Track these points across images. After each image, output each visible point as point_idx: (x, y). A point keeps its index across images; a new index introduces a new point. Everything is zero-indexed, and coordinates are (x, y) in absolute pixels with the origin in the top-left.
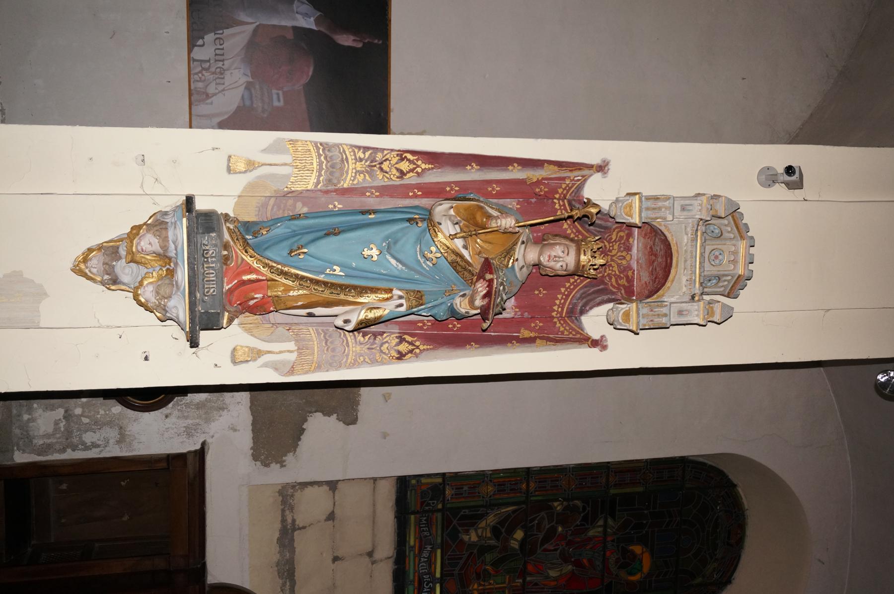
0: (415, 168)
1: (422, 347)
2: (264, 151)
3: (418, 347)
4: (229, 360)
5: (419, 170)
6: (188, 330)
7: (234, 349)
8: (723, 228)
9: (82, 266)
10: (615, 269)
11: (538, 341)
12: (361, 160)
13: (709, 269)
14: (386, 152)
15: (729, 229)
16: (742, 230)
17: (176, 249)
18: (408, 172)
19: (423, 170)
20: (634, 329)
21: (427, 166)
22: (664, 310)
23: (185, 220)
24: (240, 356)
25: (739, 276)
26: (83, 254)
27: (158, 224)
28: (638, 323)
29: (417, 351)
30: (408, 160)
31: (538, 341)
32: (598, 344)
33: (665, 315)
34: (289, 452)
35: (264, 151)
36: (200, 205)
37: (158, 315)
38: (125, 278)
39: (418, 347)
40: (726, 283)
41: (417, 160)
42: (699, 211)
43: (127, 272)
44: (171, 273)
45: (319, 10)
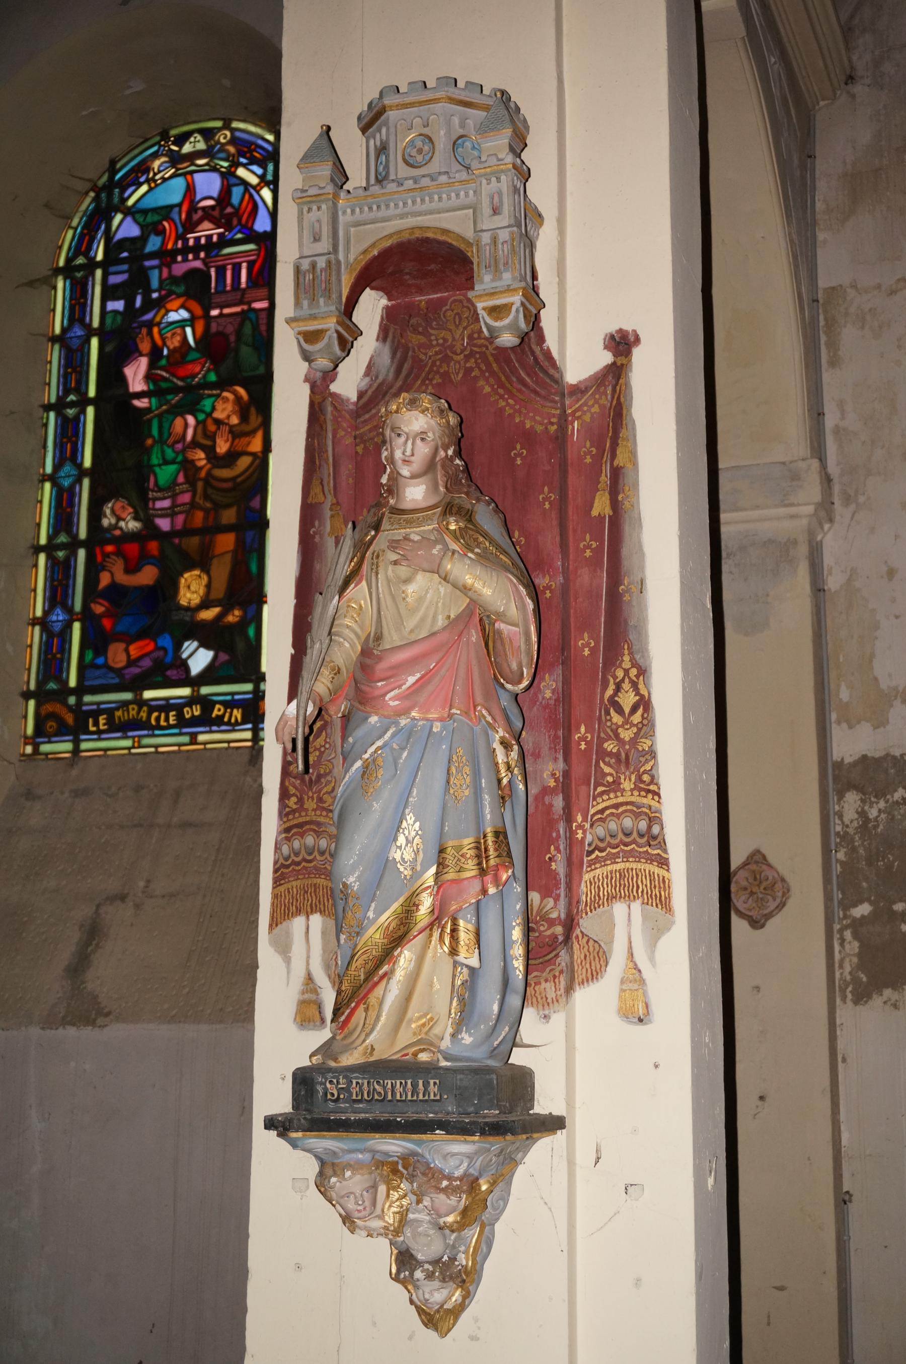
1: (627, 664)
2: (288, 961)
5: (633, 672)
11: (619, 461)
12: (300, 801)
19: (635, 664)
21: (626, 658)
22: (486, 238)
31: (619, 461)
32: (622, 344)
34: (298, 912)
35: (288, 961)
39: (626, 671)
41: (615, 677)
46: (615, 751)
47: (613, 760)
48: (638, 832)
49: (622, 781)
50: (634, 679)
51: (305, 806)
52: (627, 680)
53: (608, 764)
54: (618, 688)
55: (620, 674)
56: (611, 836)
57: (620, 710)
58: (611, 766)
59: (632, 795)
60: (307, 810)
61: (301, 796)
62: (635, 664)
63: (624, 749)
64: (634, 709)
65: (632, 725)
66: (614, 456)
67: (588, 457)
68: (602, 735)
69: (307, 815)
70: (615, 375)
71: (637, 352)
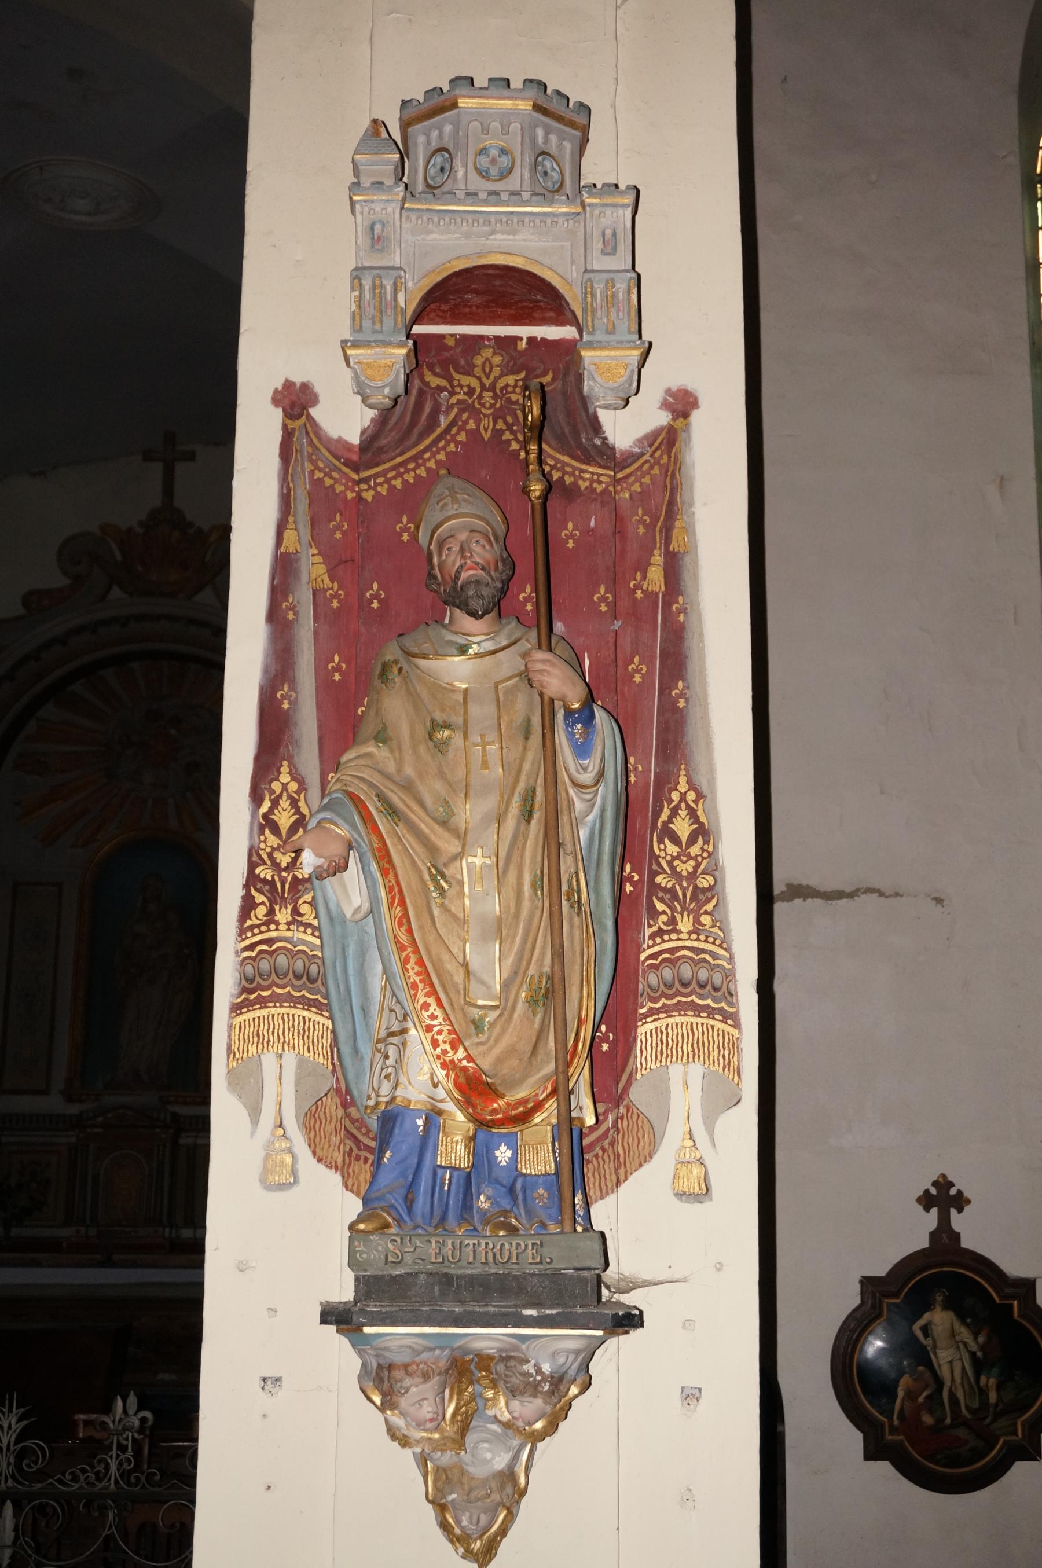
0: (290, 797)
3: (683, 797)
4: (696, 1206)
5: (691, 796)
6: (600, 1333)
7: (680, 1195)
8: (434, 145)
9: (477, 1545)
10: (510, 379)
11: (674, 546)
12: (271, 912)
13: (520, 178)
14: (255, 858)
15: (435, 134)
16: (439, 105)
17: (433, 1349)
18: (298, 811)
19: (692, 786)
20: (635, 355)
21: (683, 780)
23: (367, 1330)
24: (692, 1183)
25: (537, 107)
26: (452, 1542)
27: (382, 1380)
28: (620, 345)
29: (691, 796)
30: (271, 810)
32: (682, 404)
33: (610, 283)
36: (343, 1290)
37: (574, 1390)
38: (500, 1462)
39: (683, 797)
40: (553, 138)
41: (671, 801)
42: (386, 205)
43: (489, 1456)
44: (484, 1361)
45: (581, 357)
46: (669, 886)
47: (267, 887)
48: (698, 982)
49: (277, 912)
50: (693, 805)
51: (276, 918)
52: (683, 805)
53: (661, 900)
54: (275, 803)
55: (675, 796)
56: (665, 985)
57: (676, 840)
58: (263, 893)
59: (289, 929)
60: (277, 923)
61: (672, 914)
62: (692, 786)
63: (681, 885)
64: (692, 840)
65: (690, 858)
66: (668, 540)
67: (571, 541)
68: (655, 867)
69: (277, 929)
70: (668, 442)
71: (695, 416)
